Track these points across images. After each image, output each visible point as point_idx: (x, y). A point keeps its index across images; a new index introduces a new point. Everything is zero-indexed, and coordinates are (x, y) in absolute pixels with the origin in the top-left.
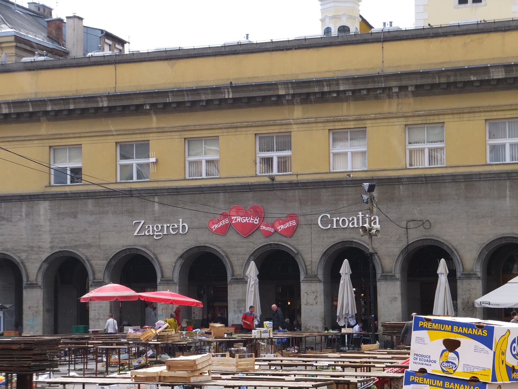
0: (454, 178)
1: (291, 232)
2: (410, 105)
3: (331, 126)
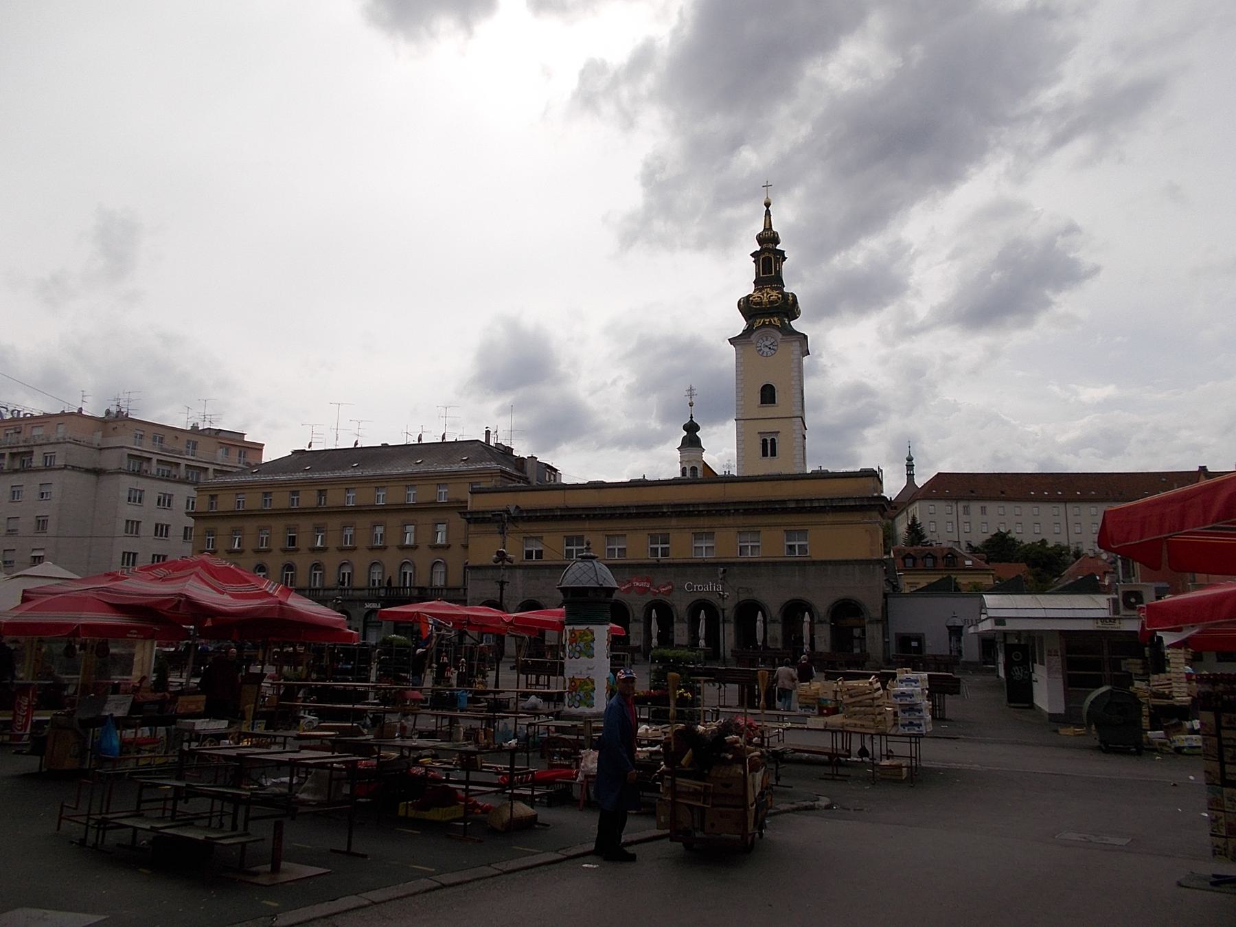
0: (766, 563)
1: (670, 591)
2: (740, 520)
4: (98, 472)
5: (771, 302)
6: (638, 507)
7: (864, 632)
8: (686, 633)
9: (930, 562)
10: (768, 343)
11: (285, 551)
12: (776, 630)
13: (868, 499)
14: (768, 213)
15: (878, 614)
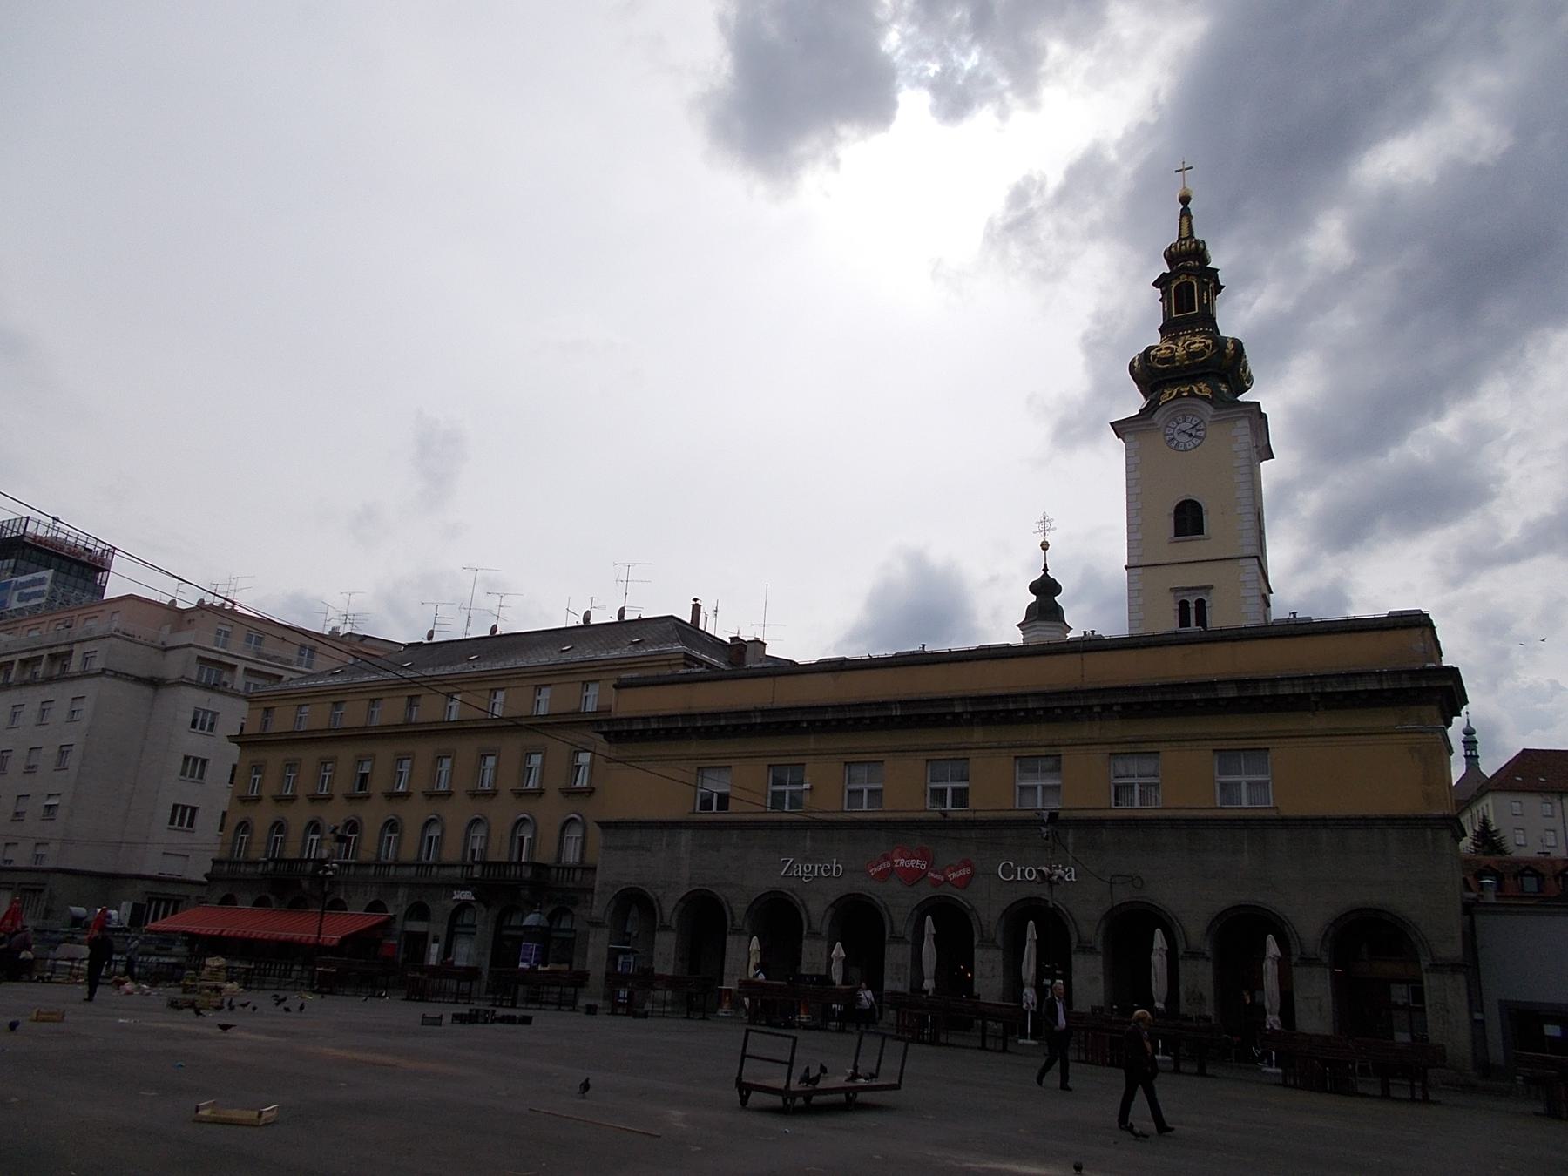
0: (1173, 824)
1: (965, 882)
2: (1116, 729)
3: (1018, 752)
4: (155, 683)
5: (1191, 355)
6: (904, 704)
7: (1418, 995)
8: (999, 970)
9: (1530, 884)
10: (1185, 427)
11: (350, 798)
12: (1200, 977)
13: (1413, 674)
14: (1186, 213)
15: (1453, 949)
